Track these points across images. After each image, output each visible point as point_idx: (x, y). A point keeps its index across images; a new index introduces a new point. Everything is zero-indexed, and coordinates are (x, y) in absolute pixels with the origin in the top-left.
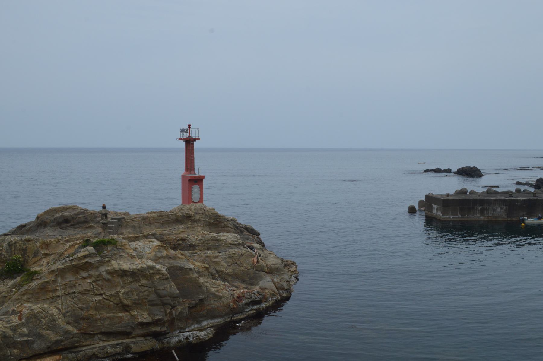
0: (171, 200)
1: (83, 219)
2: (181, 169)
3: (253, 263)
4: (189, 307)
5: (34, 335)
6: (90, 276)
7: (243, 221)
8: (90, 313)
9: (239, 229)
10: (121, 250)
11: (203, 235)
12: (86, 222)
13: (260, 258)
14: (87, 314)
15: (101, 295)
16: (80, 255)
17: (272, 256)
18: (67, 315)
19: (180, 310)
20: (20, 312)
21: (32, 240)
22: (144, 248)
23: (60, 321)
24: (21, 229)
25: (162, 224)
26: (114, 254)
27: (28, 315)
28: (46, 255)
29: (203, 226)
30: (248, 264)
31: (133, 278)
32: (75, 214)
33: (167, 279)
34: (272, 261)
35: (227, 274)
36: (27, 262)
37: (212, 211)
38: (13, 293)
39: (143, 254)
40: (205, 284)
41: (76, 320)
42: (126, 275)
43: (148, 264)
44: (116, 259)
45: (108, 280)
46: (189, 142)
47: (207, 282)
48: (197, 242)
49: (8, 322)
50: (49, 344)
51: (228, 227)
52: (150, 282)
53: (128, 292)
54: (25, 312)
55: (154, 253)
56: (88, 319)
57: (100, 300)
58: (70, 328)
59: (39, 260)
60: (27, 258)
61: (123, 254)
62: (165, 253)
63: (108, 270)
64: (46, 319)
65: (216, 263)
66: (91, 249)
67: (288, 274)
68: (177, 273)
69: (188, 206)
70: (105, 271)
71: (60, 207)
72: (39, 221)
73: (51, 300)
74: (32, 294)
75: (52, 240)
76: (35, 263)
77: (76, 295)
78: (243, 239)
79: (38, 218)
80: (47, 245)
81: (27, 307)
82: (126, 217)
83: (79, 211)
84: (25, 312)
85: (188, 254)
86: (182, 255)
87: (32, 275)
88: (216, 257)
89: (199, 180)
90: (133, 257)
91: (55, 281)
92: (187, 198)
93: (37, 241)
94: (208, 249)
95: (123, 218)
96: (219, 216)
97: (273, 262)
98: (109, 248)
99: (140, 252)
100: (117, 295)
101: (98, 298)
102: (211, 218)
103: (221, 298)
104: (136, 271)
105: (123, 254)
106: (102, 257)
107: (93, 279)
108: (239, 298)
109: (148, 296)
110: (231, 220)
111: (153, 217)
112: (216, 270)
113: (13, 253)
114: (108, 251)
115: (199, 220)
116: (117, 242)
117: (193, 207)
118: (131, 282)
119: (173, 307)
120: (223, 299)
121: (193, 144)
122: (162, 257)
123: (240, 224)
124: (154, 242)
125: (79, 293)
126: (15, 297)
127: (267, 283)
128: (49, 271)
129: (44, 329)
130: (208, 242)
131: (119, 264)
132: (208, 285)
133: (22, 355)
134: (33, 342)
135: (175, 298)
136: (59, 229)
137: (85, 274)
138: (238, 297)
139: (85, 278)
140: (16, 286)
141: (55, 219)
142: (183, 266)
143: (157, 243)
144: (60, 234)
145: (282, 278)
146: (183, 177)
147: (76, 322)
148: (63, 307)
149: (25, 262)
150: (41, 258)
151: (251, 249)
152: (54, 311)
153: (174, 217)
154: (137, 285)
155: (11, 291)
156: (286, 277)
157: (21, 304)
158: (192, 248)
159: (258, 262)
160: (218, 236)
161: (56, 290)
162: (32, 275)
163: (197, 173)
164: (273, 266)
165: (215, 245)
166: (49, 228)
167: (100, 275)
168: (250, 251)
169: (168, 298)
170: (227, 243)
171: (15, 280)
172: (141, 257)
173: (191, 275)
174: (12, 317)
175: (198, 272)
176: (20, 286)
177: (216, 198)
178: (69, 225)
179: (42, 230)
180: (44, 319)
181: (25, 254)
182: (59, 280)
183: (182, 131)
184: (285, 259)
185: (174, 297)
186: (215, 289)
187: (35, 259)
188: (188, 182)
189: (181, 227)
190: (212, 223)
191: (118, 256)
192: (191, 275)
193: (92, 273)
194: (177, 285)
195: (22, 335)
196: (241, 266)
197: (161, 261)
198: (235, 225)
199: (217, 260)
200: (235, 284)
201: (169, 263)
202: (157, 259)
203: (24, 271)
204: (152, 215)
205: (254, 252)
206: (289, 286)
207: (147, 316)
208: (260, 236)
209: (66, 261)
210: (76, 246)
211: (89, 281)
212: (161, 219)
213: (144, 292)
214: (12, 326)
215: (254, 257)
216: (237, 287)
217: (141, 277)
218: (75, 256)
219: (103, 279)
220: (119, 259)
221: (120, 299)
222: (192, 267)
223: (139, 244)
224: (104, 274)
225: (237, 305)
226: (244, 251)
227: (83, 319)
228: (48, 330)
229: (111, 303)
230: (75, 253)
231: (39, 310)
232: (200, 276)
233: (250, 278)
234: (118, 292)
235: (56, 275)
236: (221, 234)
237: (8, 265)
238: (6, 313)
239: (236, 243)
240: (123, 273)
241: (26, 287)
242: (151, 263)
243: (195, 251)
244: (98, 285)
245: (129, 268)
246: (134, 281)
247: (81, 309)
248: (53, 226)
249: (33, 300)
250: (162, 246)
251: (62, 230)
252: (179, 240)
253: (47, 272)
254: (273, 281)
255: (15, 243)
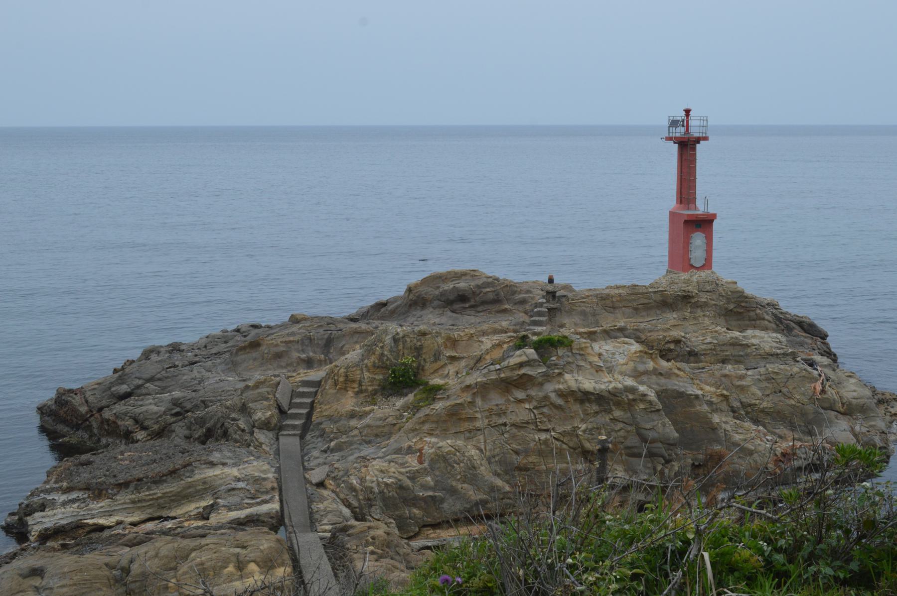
0: (646, 261)
1: (491, 296)
2: (670, 200)
3: (814, 392)
4: (693, 464)
5: (444, 490)
6: (529, 399)
7: (792, 307)
8: (531, 459)
9: (786, 324)
10: (578, 357)
11: (715, 334)
12: (497, 301)
13: (828, 384)
14: (525, 461)
15: (547, 430)
16: (513, 361)
17: (853, 381)
18: (493, 460)
19: (677, 468)
20: (420, 450)
21: (431, 333)
22: (614, 354)
23: (484, 470)
24: (379, 311)
25: (636, 309)
26: (569, 363)
27: (433, 456)
28: (453, 359)
29: (715, 316)
30: (804, 394)
31: (600, 405)
32: (478, 286)
33: (658, 410)
34: (851, 391)
35: (763, 411)
36: (423, 370)
37: (731, 286)
38: (404, 420)
39: (612, 363)
40: (724, 425)
41: (509, 470)
42: (589, 401)
43: (626, 383)
44: (571, 372)
45: (558, 407)
46: (687, 146)
47: (726, 423)
48: (704, 347)
49: (402, 465)
50: (468, 506)
51: (764, 319)
52: (629, 415)
53: (591, 429)
54: (428, 451)
55: (631, 364)
56: (527, 469)
57: (546, 440)
58: (499, 482)
59: (442, 367)
60: (422, 362)
61: (582, 363)
62: (651, 365)
63: (560, 390)
64: (462, 465)
65: (742, 388)
66: (531, 352)
67: (884, 420)
68: (674, 402)
69: (684, 276)
70: (555, 391)
71: (449, 273)
72: (411, 296)
73: (468, 435)
74: (437, 422)
75: (462, 334)
76: (436, 371)
77: (508, 428)
78: (792, 344)
79: (409, 290)
80: (453, 343)
81: (432, 444)
82: (570, 295)
83: (485, 279)
84: (428, 451)
85: (688, 369)
86: (679, 369)
87: (433, 392)
88: (742, 377)
89: (704, 223)
90: (599, 369)
91: (472, 403)
92: (680, 258)
93: (438, 334)
94: (724, 362)
95: (564, 296)
96: (746, 297)
97: (855, 394)
98: (561, 352)
99: (607, 361)
100: (573, 433)
101: (544, 436)
102: (729, 300)
103: (751, 453)
104: (606, 394)
105: (582, 363)
106: (548, 367)
107: (535, 403)
108: (786, 456)
109: (625, 438)
110: (768, 304)
111: (620, 295)
112: (741, 403)
113: (401, 353)
114: (559, 357)
115: (706, 304)
116: (572, 341)
117: (695, 278)
118: (597, 413)
119: (668, 461)
120: (755, 455)
121: (694, 149)
122: (646, 373)
123: (786, 313)
124: (631, 344)
125: (513, 425)
126: (409, 425)
127: (841, 432)
128: (463, 386)
129: (458, 480)
130: (724, 348)
131: (576, 380)
132: (728, 428)
133: (425, 519)
134: (442, 500)
135: (672, 445)
136: (450, 313)
137: (520, 395)
138: (784, 455)
139: (521, 401)
140: (409, 408)
141: (442, 294)
142: (683, 390)
143: (636, 347)
144: (451, 322)
145: (871, 426)
146: (673, 215)
147: (507, 474)
148: (488, 448)
149: (420, 369)
150: (446, 364)
151: (811, 365)
152: (473, 452)
153: (658, 297)
154: (607, 419)
155: (402, 416)
156: (881, 424)
157: (421, 439)
158: (692, 359)
159: (823, 391)
160: (744, 337)
161: (473, 419)
162: (433, 392)
163: (700, 208)
164: (854, 402)
165: (739, 353)
166: (431, 309)
167: (546, 398)
168: (809, 369)
169: (660, 445)
170: (762, 352)
171: (406, 399)
172: (610, 370)
173: (698, 408)
174: (408, 458)
175: (710, 403)
176: (415, 408)
177: (736, 260)
178: (467, 305)
179: (418, 313)
180: (458, 464)
181: (419, 356)
182: (479, 402)
183: (674, 123)
184: (879, 386)
185: (668, 444)
186: (741, 437)
187: (436, 366)
188: (682, 225)
189: (671, 317)
190: (731, 310)
191: (574, 366)
192: (698, 408)
193: (533, 392)
194: (675, 423)
195: (424, 487)
196: (789, 398)
197: (644, 378)
198: (775, 316)
199: (743, 383)
200: (777, 431)
201: (658, 384)
202: (637, 375)
203: (418, 385)
204: (617, 291)
205: (816, 372)
206: (886, 441)
207: (623, 473)
208: (828, 340)
209: (490, 371)
210: (505, 346)
211: (527, 406)
212: (634, 300)
213: (619, 430)
214: (409, 472)
215: (817, 380)
216: (780, 437)
217: (614, 405)
218: (505, 364)
219: (552, 404)
220: (575, 371)
221: (580, 441)
222: (700, 392)
223: (604, 347)
224: (553, 396)
225: (781, 469)
226: (796, 369)
227: (520, 469)
228: (464, 482)
229: (564, 446)
230: (503, 359)
231: (450, 448)
232: (713, 411)
233: (806, 422)
234: (576, 429)
235: (474, 394)
236: (749, 332)
237: (393, 372)
238: (398, 451)
239: (779, 351)
240: (584, 397)
241: (425, 411)
242: (630, 382)
243: (701, 365)
244: (542, 414)
245: (594, 388)
246: (601, 411)
247: (517, 453)
248: (439, 307)
249: (438, 432)
250: (646, 353)
251: (454, 315)
252: (668, 342)
253: (458, 387)
254: (852, 430)
255: (403, 337)
